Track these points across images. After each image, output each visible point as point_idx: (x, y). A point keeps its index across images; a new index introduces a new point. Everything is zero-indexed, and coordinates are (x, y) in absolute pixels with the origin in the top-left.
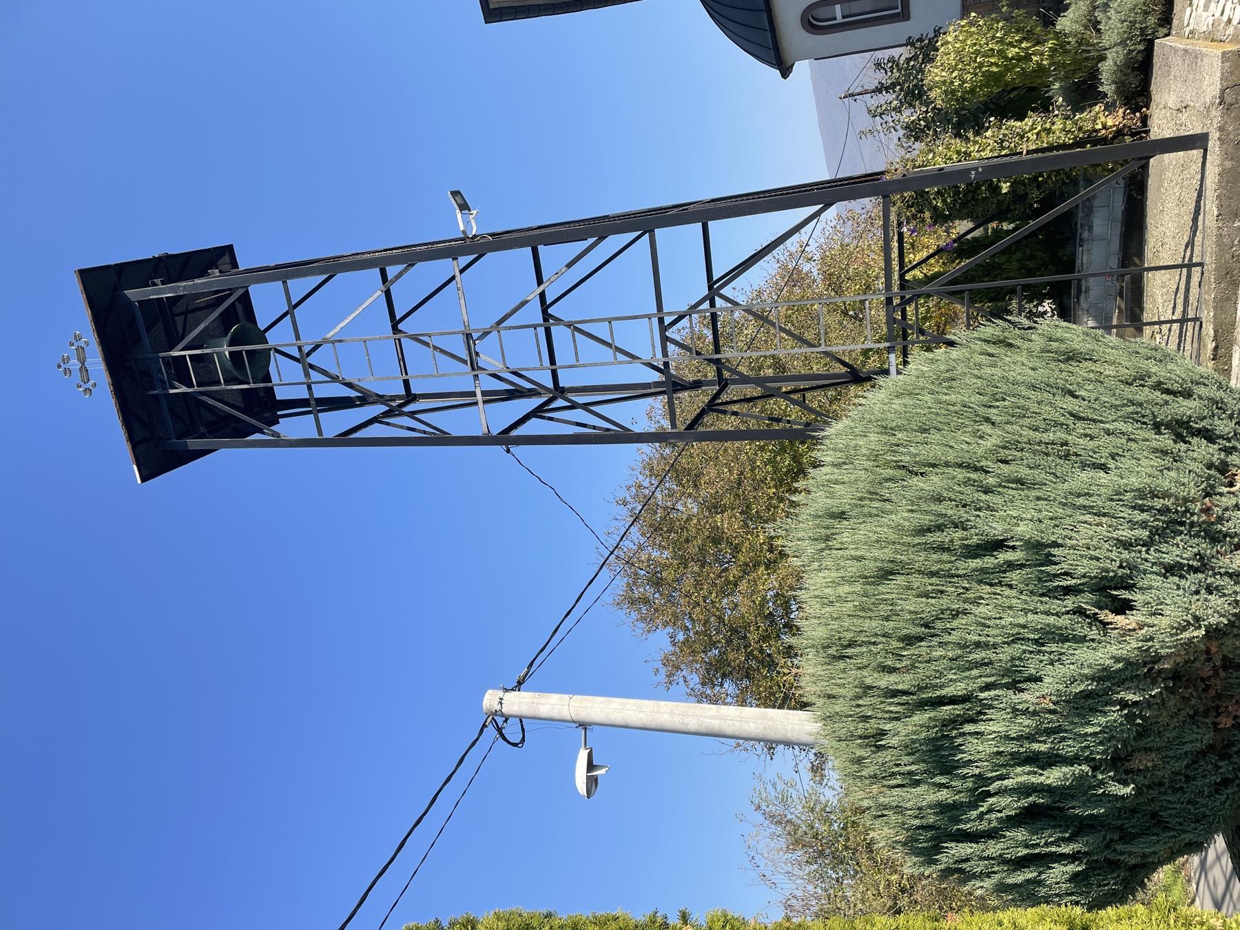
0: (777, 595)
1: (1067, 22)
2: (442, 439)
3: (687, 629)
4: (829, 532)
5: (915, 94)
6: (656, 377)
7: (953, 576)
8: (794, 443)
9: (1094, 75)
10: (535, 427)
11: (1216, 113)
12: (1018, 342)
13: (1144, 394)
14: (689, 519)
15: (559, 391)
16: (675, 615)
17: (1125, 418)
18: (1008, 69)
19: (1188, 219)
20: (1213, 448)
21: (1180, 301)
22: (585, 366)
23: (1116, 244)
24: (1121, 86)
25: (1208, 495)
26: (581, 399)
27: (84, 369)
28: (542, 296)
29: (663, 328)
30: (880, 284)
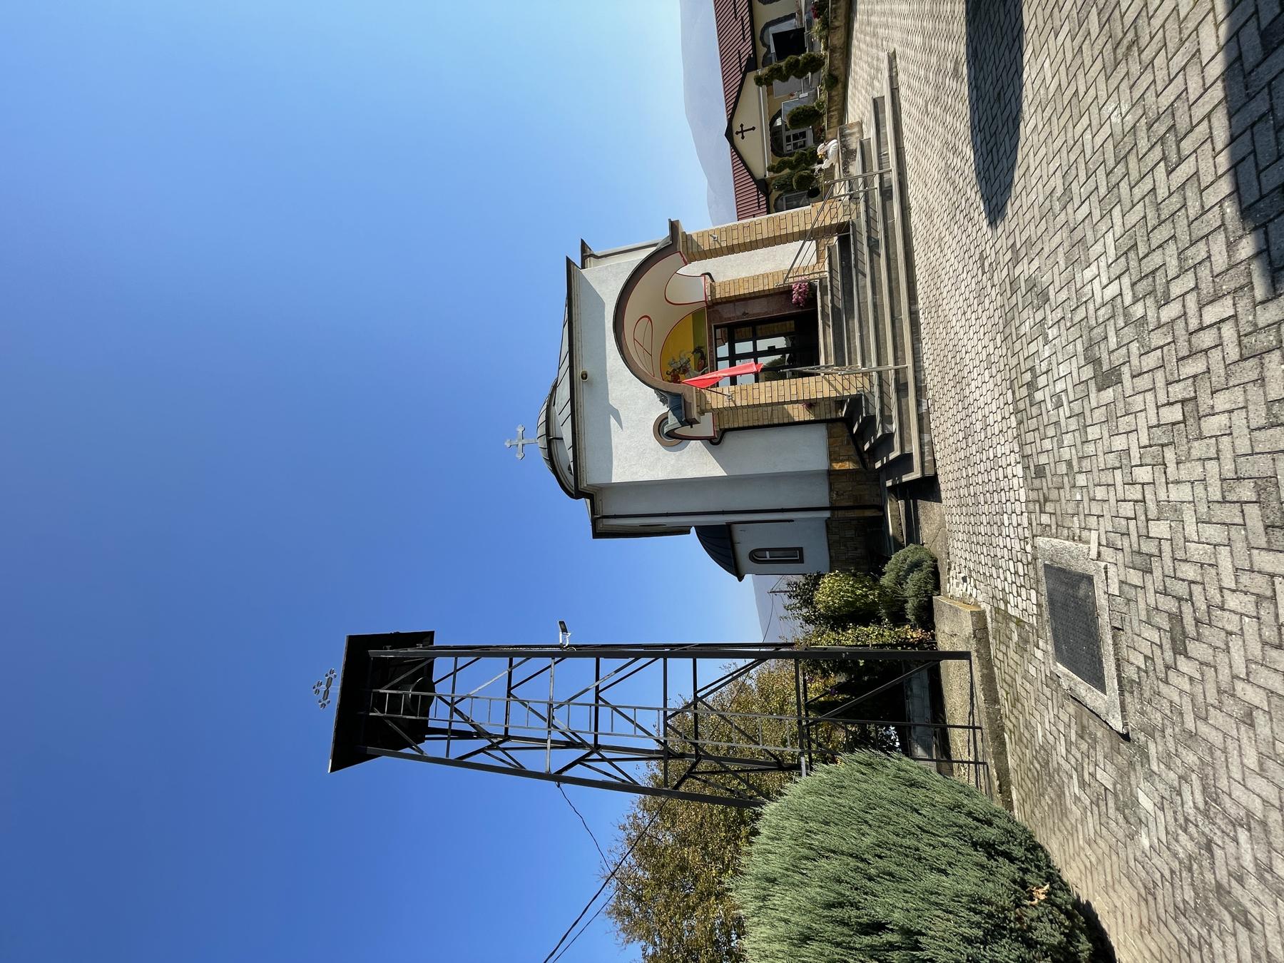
0: (722, 923)
1: (885, 581)
2: (519, 771)
3: (655, 944)
4: (765, 893)
5: (808, 602)
6: (655, 746)
7: (852, 949)
8: (743, 808)
9: (903, 609)
10: (579, 772)
11: (973, 642)
12: (880, 768)
13: (963, 820)
14: (666, 848)
15: (597, 747)
16: (648, 931)
17: (954, 835)
18: (857, 600)
19: (967, 698)
20: (1014, 867)
21: (972, 748)
22: (616, 732)
23: (927, 702)
24: (918, 618)
25: (1017, 906)
26: (608, 755)
27: (327, 692)
28: (597, 687)
29: (666, 718)
30: (793, 699)
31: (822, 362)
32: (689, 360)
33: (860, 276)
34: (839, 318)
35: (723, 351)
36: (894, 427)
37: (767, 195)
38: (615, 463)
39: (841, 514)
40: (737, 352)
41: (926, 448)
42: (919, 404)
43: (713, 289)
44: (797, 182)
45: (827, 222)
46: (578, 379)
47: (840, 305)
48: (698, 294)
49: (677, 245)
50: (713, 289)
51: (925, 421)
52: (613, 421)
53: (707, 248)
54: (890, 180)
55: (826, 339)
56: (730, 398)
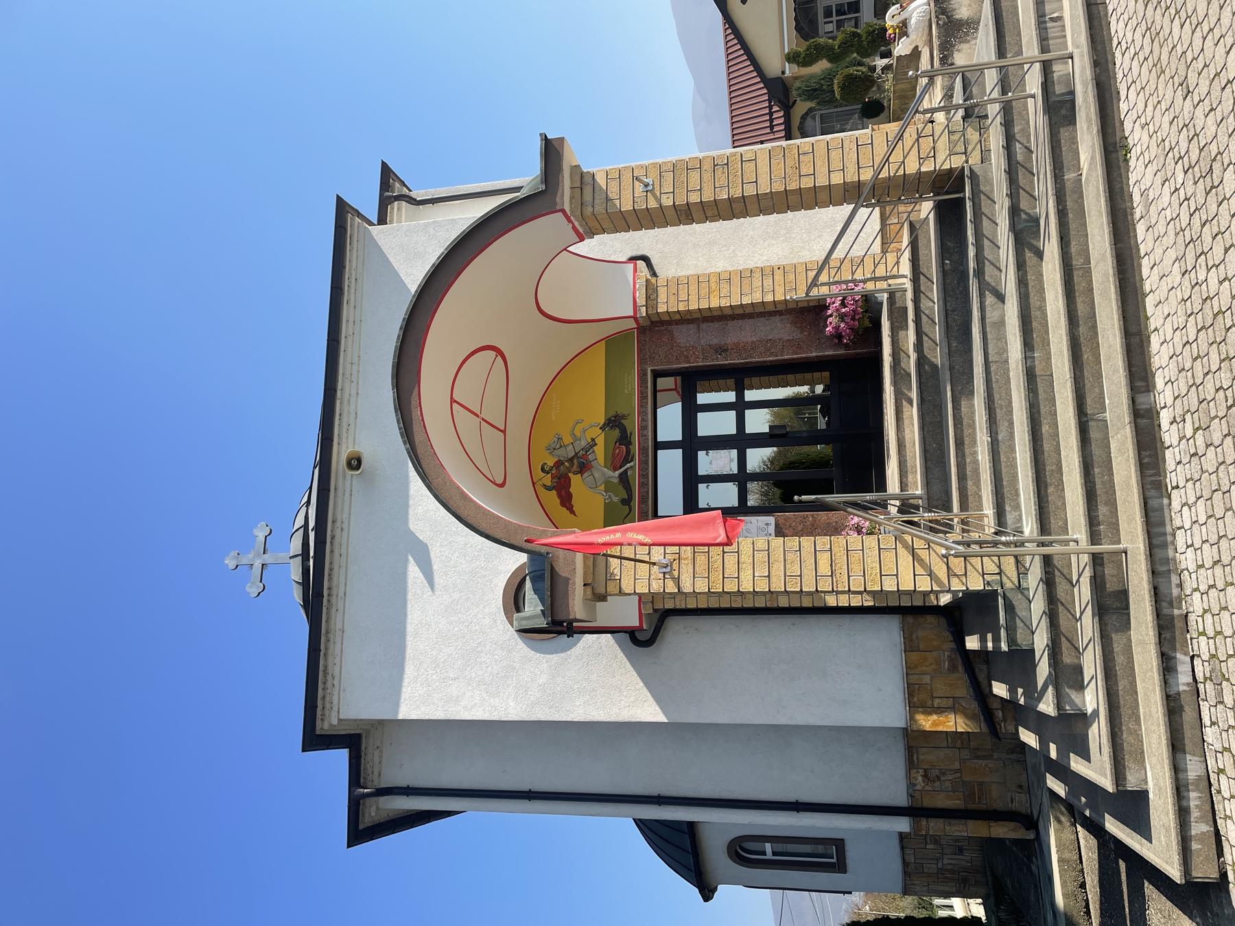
31: (893, 485)
32: (593, 443)
33: (990, 299)
34: (940, 387)
35: (670, 421)
36: (1092, 699)
37: (787, 107)
38: (409, 670)
39: (935, 826)
40: (702, 432)
41: (1194, 799)
42: (1167, 667)
43: (651, 291)
44: (843, 88)
45: (912, 167)
46: (329, 466)
47: (937, 356)
48: (618, 302)
49: (558, 192)
50: (651, 291)
51: (1188, 715)
52: (414, 572)
53: (627, 206)
54: (1069, 80)
55: (901, 428)
56: (667, 570)
